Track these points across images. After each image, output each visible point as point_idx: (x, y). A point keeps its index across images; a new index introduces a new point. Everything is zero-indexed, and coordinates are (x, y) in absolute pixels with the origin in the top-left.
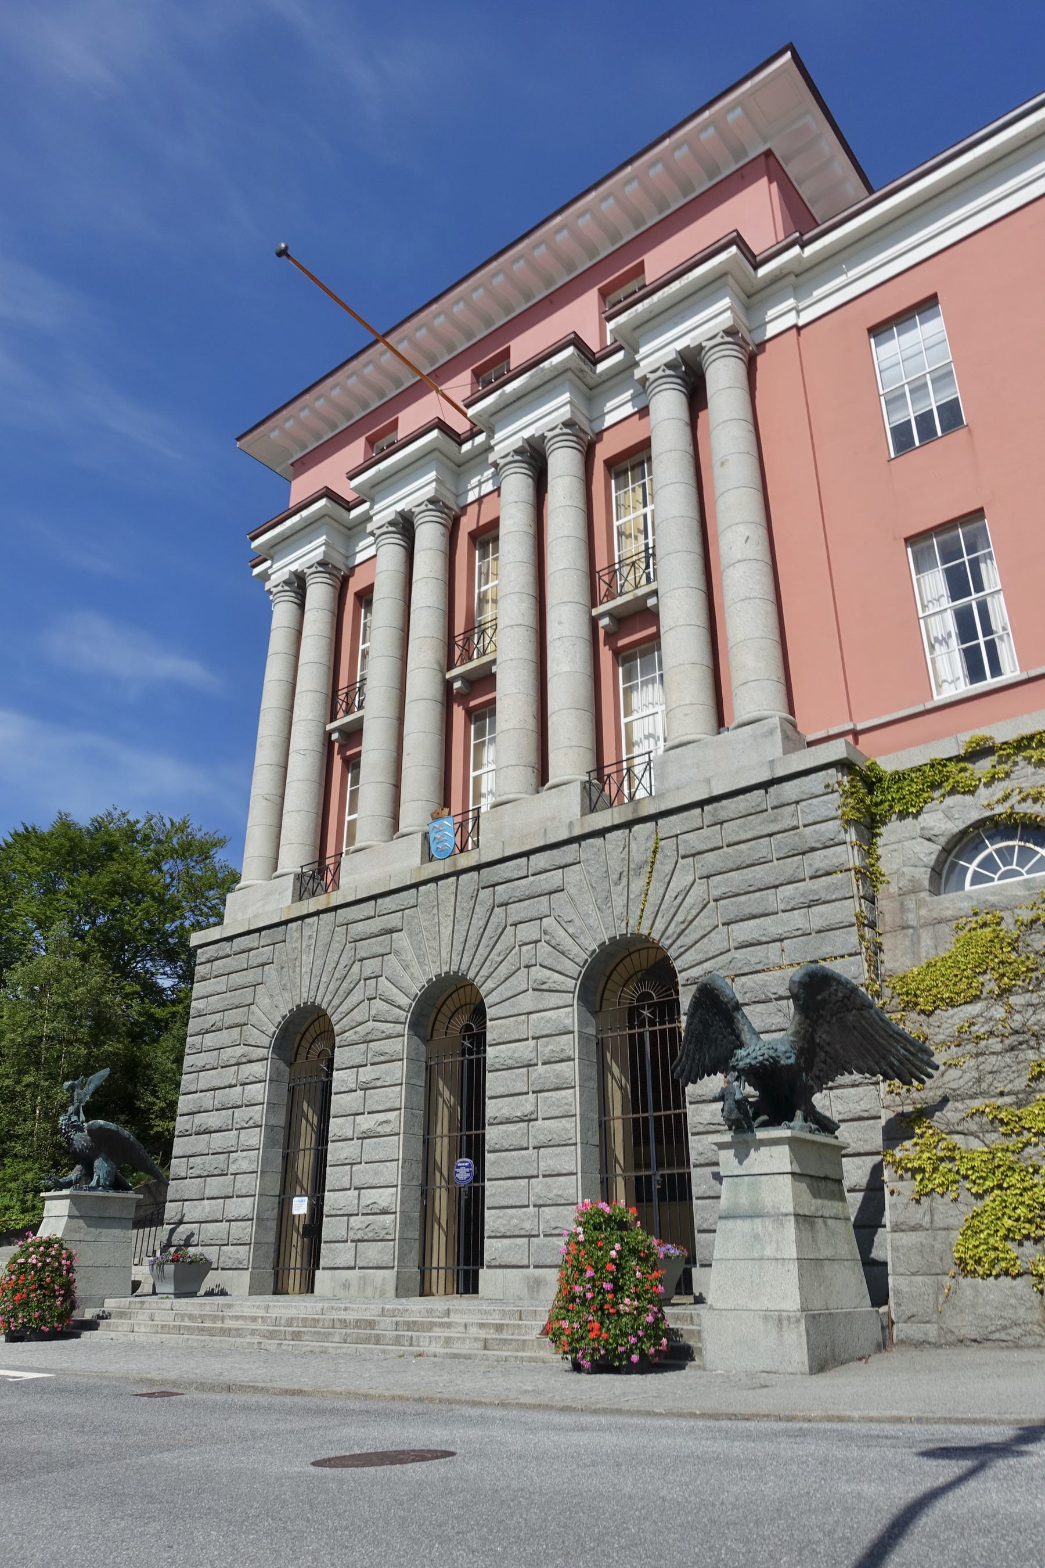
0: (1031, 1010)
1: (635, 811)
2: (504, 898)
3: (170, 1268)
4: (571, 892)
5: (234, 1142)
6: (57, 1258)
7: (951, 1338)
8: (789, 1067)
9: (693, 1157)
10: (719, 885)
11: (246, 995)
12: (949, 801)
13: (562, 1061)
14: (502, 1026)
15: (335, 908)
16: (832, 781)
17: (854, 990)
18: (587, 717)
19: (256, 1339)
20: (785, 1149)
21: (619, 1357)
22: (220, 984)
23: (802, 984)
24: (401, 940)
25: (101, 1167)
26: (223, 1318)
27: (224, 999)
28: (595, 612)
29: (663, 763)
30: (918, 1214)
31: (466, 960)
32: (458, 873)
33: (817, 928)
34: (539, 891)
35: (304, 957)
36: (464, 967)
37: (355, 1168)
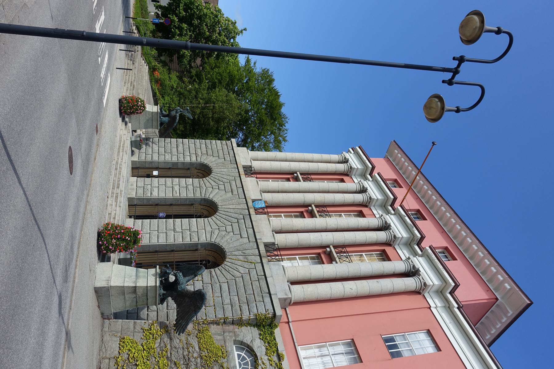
1: (264, 257)
3: (139, 139)
6: (140, 109)
7: (104, 334)
8: (177, 288)
11: (216, 154)
12: (264, 348)
15: (240, 177)
16: (269, 311)
19: (116, 159)
20: (154, 285)
21: (101, 239)
25: (166, 119)
28: (331, 246)
30: (138, 328)
31: (222, 212)
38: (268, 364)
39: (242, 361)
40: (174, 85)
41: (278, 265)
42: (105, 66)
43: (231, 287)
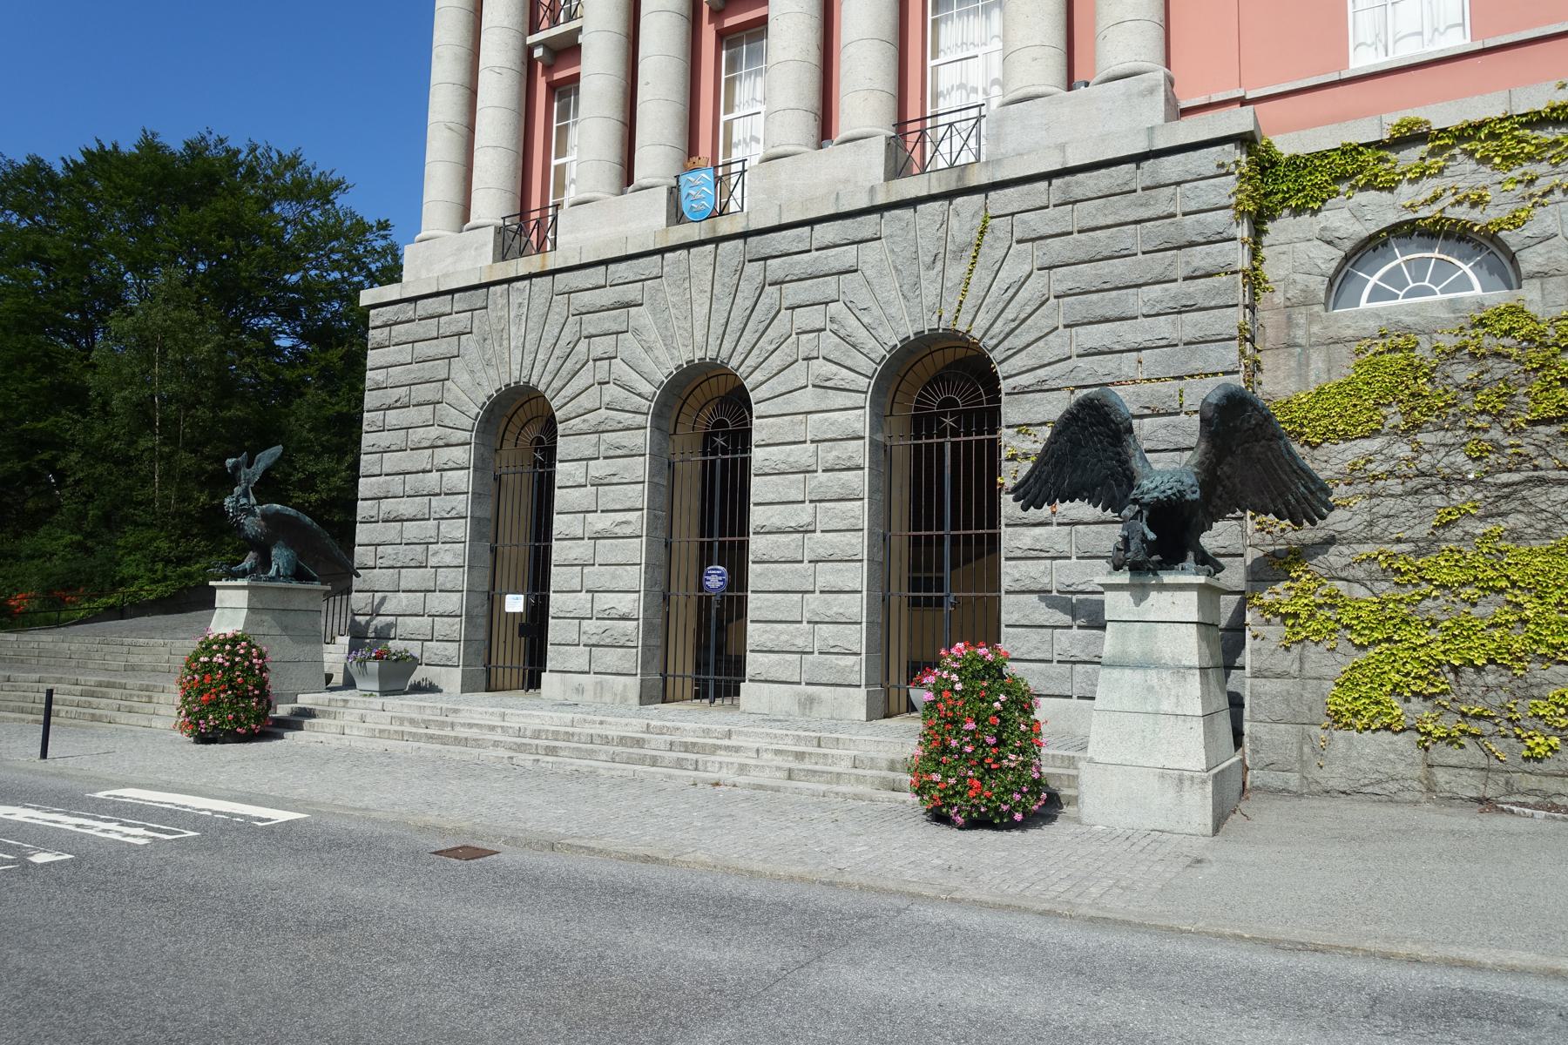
0: (1443, 451)
1: (960, 178)
2: (780, 275)
4: (867, 273)
5: (434, 533)
9: (1006, 583)
10: (1063, 279)
11: (440, 369)
13: (849, 469)
14: (773, 425)
17: (1269, 417)
18: (892, 51)
20: (1194, 595)
22: (404, 353)
23: (1219, 408)
24: (642, 317)
25: (280, 557)
26: (453, 725)
27: (410, 372)
29: (1000, 122)
32: (717, 241)
33: (1186, 339)
34: (826, 270)
35: (513, 329)
36: (724, 354)
37: (586, 570)
38: (1434, 181)
39: (1402, 284)
40: (68, 538)
41: (1000, 122)
42: (68, 822)
43: (1099, 312)
